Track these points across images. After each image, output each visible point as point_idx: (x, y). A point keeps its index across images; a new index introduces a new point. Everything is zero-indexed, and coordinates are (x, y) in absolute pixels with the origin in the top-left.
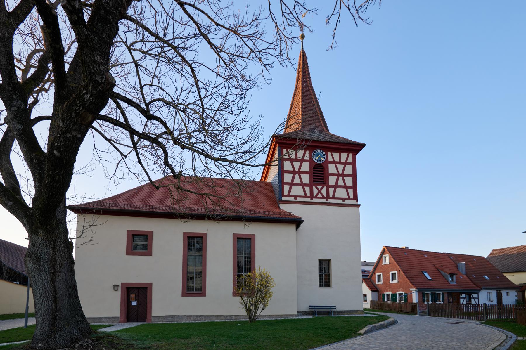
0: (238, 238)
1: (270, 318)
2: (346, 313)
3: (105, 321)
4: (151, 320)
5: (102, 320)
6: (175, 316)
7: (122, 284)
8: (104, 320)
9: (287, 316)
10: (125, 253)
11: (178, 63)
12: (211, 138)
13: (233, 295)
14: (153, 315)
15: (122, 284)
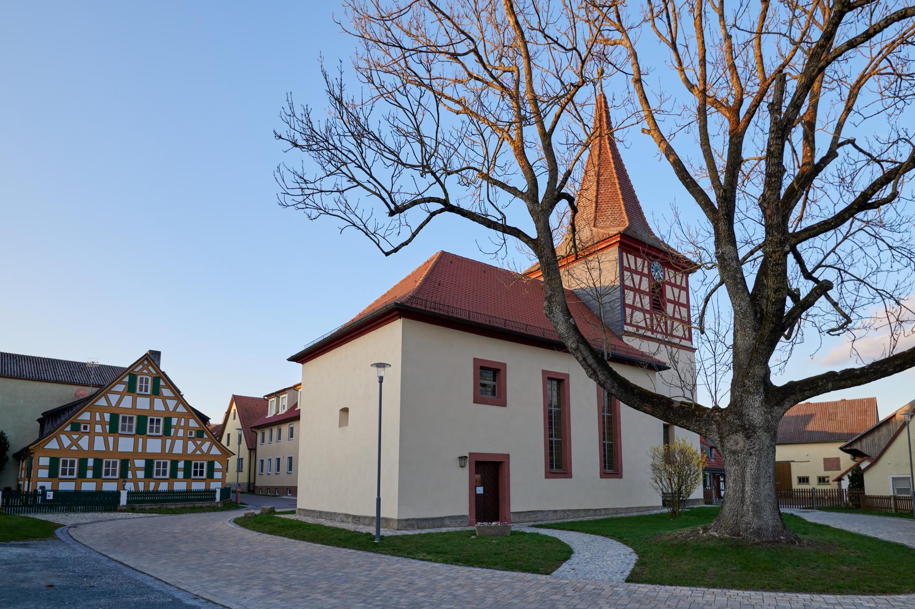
0: (482, 368)
1: (607, 515)
2: (690, 504)
3: (449, 523)
4: (510, 519)
5: (446, 523)
6: (538, 511)
7: (470, 454)
8: (583, 514)
9: (648, 508)
10: (471, 399)
11: (881, 296)
12: (317, 136)
13: (601, 477)
14: (512, 510)
15: (470, 454)
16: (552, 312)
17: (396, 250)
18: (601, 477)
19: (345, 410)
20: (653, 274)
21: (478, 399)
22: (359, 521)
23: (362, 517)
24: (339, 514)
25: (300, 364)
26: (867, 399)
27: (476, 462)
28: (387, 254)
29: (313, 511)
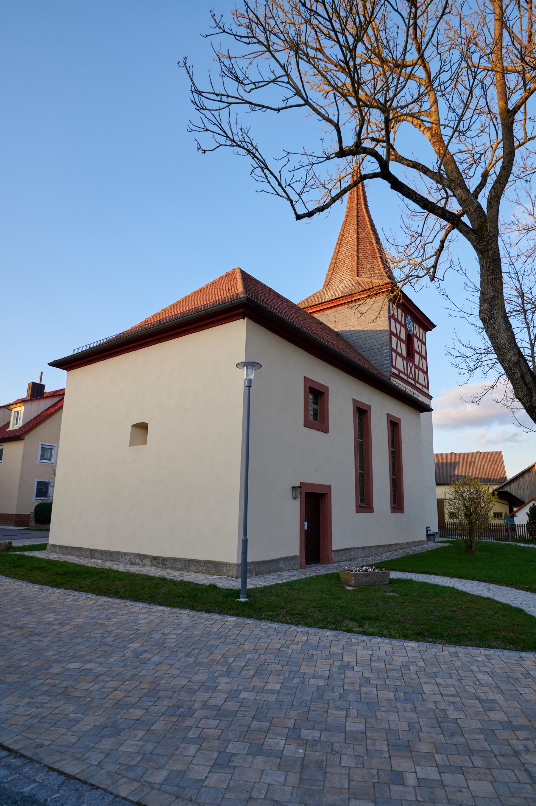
16: (493, 317)
17: (310, 214)
18: (391, 512)
19: (143, 427)
20: (407, 325)
21: (307, 424)
22: (164, 564)
23: (168, 559)
24: (126, 554)
25: (65, 372)
26: (496, 452)
27: (306, 493)
28: (299, 217)
29: (79, 549)
